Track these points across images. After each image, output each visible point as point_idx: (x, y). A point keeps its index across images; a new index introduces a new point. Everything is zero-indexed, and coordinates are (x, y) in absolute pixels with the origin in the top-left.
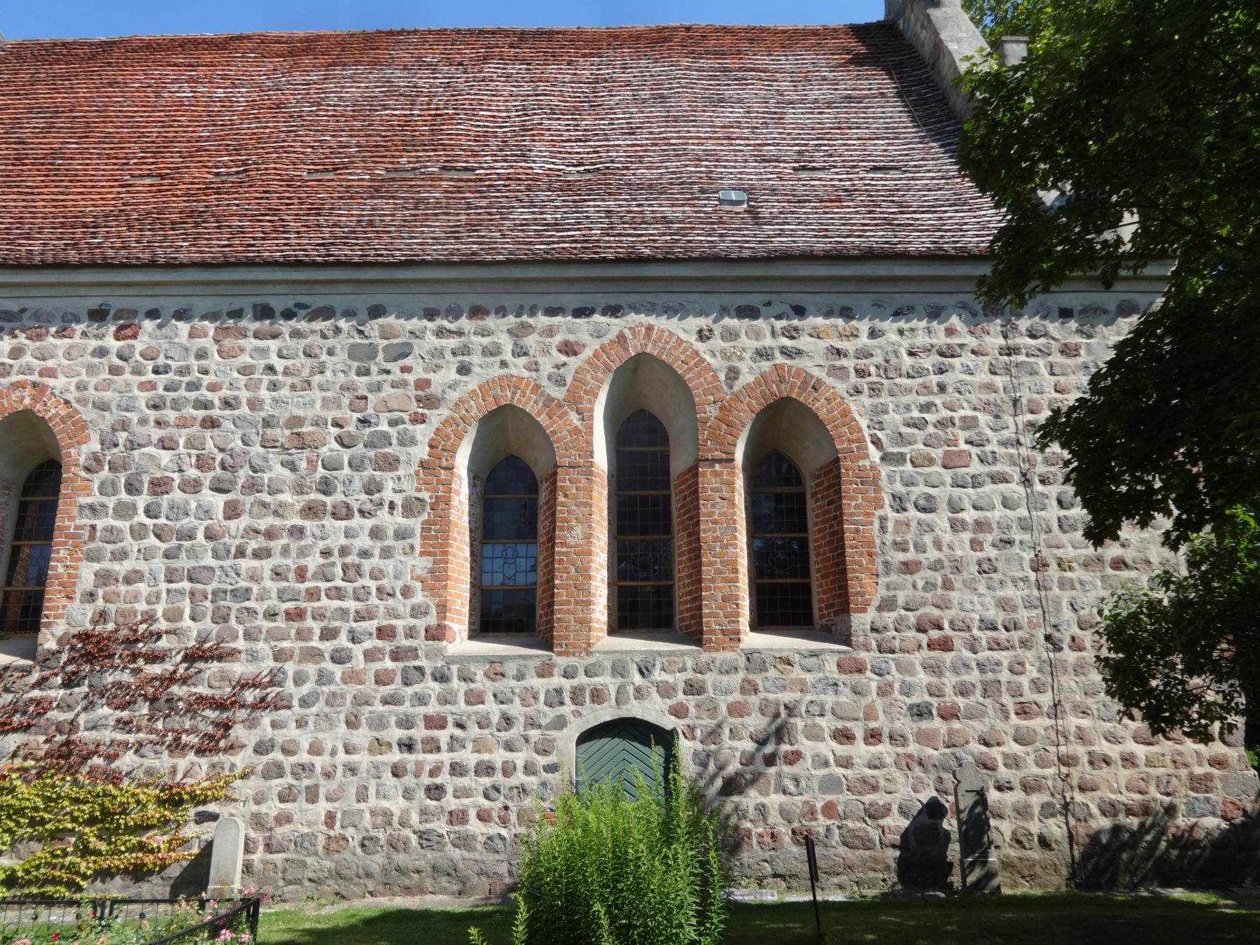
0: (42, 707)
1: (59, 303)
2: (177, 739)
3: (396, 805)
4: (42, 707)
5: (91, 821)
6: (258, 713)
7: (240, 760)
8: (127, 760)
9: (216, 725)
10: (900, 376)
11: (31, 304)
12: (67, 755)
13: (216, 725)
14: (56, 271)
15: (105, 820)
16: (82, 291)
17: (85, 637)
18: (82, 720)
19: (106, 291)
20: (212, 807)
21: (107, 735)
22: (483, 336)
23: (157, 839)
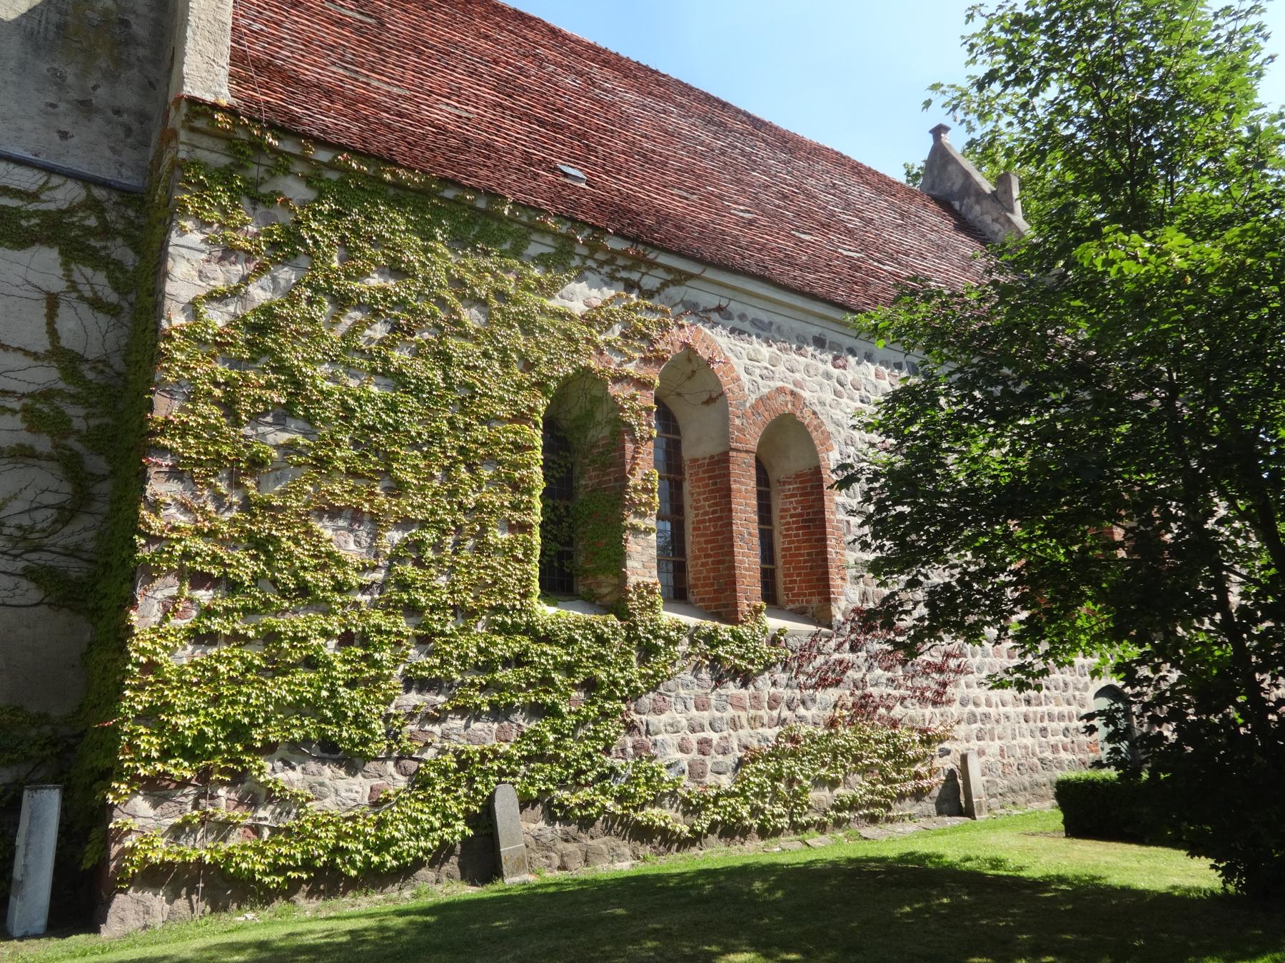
0: (844, 667)
1: (795, 324)
2: (922, 694)
3: (1028, 741)
4: (844, 667)
5: (889, 756)
6: (958, 676)
7: (955, 709)
8: (898, 711)
9: (939, 684)
10: (763, 725)
11: (778, 319)
12: (864, 706)
13: (939, 684)
14: (759, 284)
15: (897, 754)
16: (810, 319)
17: (857, 611)
18: (867, 678)
19: (824, 323)
20: (946, 745)
21: (886, 691)
22: (444, 300)
23: (920, 768)
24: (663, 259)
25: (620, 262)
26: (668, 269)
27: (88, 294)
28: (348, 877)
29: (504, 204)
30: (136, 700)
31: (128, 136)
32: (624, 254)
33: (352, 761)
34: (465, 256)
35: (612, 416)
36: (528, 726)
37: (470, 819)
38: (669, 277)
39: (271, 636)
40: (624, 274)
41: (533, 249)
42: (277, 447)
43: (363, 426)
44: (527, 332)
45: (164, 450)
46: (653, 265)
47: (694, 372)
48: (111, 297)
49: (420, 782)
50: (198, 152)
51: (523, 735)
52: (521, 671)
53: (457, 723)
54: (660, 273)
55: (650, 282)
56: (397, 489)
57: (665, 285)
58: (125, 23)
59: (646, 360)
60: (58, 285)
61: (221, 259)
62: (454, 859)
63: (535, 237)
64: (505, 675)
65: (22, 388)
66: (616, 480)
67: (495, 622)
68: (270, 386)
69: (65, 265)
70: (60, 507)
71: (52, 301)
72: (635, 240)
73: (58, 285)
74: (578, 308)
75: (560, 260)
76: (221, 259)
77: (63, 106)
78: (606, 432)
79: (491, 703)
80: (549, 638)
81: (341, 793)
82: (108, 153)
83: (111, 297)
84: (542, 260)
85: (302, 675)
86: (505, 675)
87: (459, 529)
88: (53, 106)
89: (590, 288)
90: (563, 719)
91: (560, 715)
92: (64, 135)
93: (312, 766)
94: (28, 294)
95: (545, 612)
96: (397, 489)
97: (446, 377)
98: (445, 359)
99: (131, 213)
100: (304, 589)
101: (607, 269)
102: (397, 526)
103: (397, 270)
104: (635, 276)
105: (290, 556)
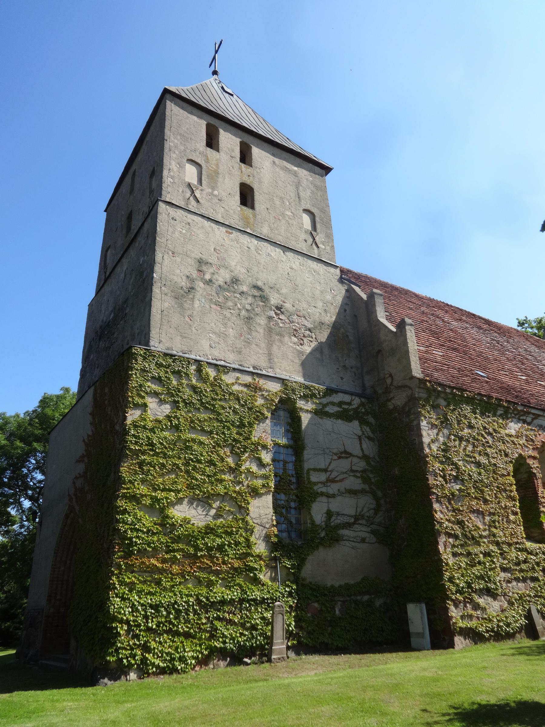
24: (533, 411)
25: (522, 413)
26: (534, 414)
27: (367, 435)
28: (502, 635)
29: (492, 399)
30: (447, 575)
31: (355, 375)
32: (522, 411)
33: (494, 596)
34: (484, 418)
35: (528, 470)
36: (532, 585)
37: (526, 617)
38: (533, 417)
39: (469, 554)
40: (522, 418)
41: (499, 412)
42: (457, 490)
43: (475, 481)
44: (504, 443)
45: (434, 493)
46: (529, 413)
47: (543, 450)
48: (371, 435)
49: (511, 603)
50: (420, 394)
51: (531, 588)
52: (527, 565)
53: (514, 583)
54: (531, 416)
55: (529, 419)
56: (486, 501)
57: (533, 419)
58: (347, 336)
59: (533, 449)
60: (360, 433)
61: (431, 428)
62: (523, 631)
63: (499, 408)
64: (524, 566)
65: (360, 469)
66: (533, 494)
67: (517, 548)
68: (452, 470)
69: (360, 426)
70: (374, 509)
71: (360, 438)
72: (525, 406)
73: (360, 433)
74: (513, 432)
75: (505, 416)
76: (431, 428)
77: (340, 368)
78: (525, 476)
79: (522, 577)
80: (531, 553)
81: (493, 607)
82: (352, 383)
83: (371, 435)
84: (501, 416)
85: (479, 567)
86: (524, 566)
87: (503, 516)
88: (338, 369)
89: (515, 424)
90: (540, 582)
91: (539, 580)
92: (342, 378)
93: (486, 597)
94: (353, 437)
95: (529, 545)
96: (486, 501)
97: (489, 462)
98: (487, 455)
99: (371, 406)
100: (473, 538)
101: (517, 417)
102: (489, 515)
103: (471, 427)
104: (524, 418)
105: (468, 527)
